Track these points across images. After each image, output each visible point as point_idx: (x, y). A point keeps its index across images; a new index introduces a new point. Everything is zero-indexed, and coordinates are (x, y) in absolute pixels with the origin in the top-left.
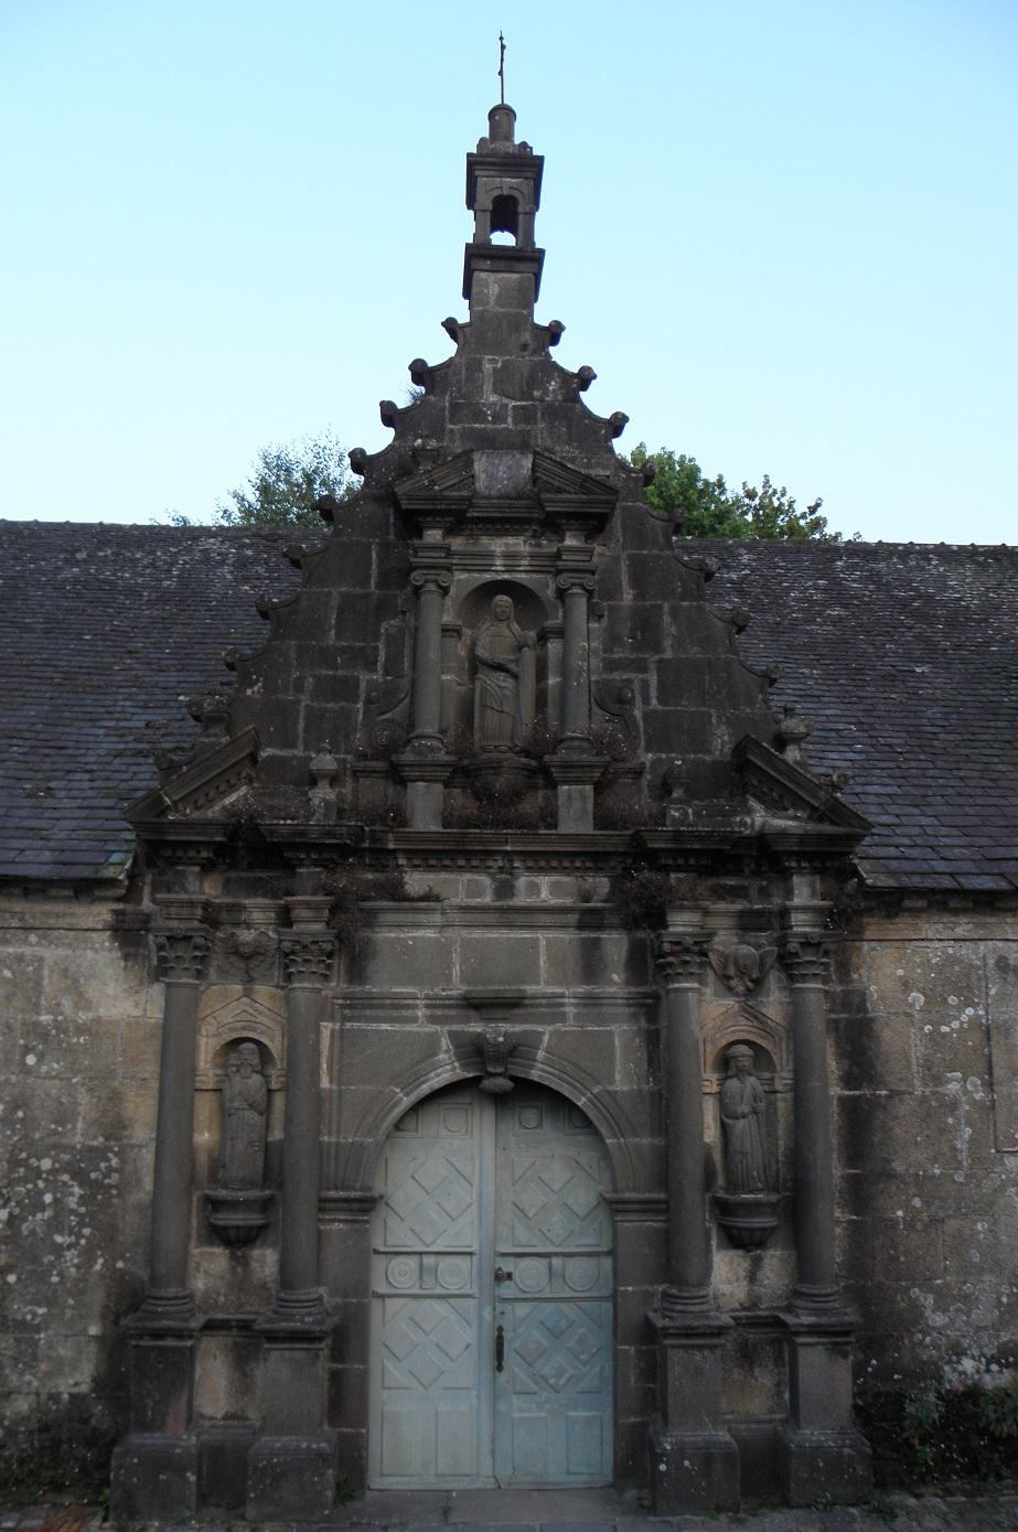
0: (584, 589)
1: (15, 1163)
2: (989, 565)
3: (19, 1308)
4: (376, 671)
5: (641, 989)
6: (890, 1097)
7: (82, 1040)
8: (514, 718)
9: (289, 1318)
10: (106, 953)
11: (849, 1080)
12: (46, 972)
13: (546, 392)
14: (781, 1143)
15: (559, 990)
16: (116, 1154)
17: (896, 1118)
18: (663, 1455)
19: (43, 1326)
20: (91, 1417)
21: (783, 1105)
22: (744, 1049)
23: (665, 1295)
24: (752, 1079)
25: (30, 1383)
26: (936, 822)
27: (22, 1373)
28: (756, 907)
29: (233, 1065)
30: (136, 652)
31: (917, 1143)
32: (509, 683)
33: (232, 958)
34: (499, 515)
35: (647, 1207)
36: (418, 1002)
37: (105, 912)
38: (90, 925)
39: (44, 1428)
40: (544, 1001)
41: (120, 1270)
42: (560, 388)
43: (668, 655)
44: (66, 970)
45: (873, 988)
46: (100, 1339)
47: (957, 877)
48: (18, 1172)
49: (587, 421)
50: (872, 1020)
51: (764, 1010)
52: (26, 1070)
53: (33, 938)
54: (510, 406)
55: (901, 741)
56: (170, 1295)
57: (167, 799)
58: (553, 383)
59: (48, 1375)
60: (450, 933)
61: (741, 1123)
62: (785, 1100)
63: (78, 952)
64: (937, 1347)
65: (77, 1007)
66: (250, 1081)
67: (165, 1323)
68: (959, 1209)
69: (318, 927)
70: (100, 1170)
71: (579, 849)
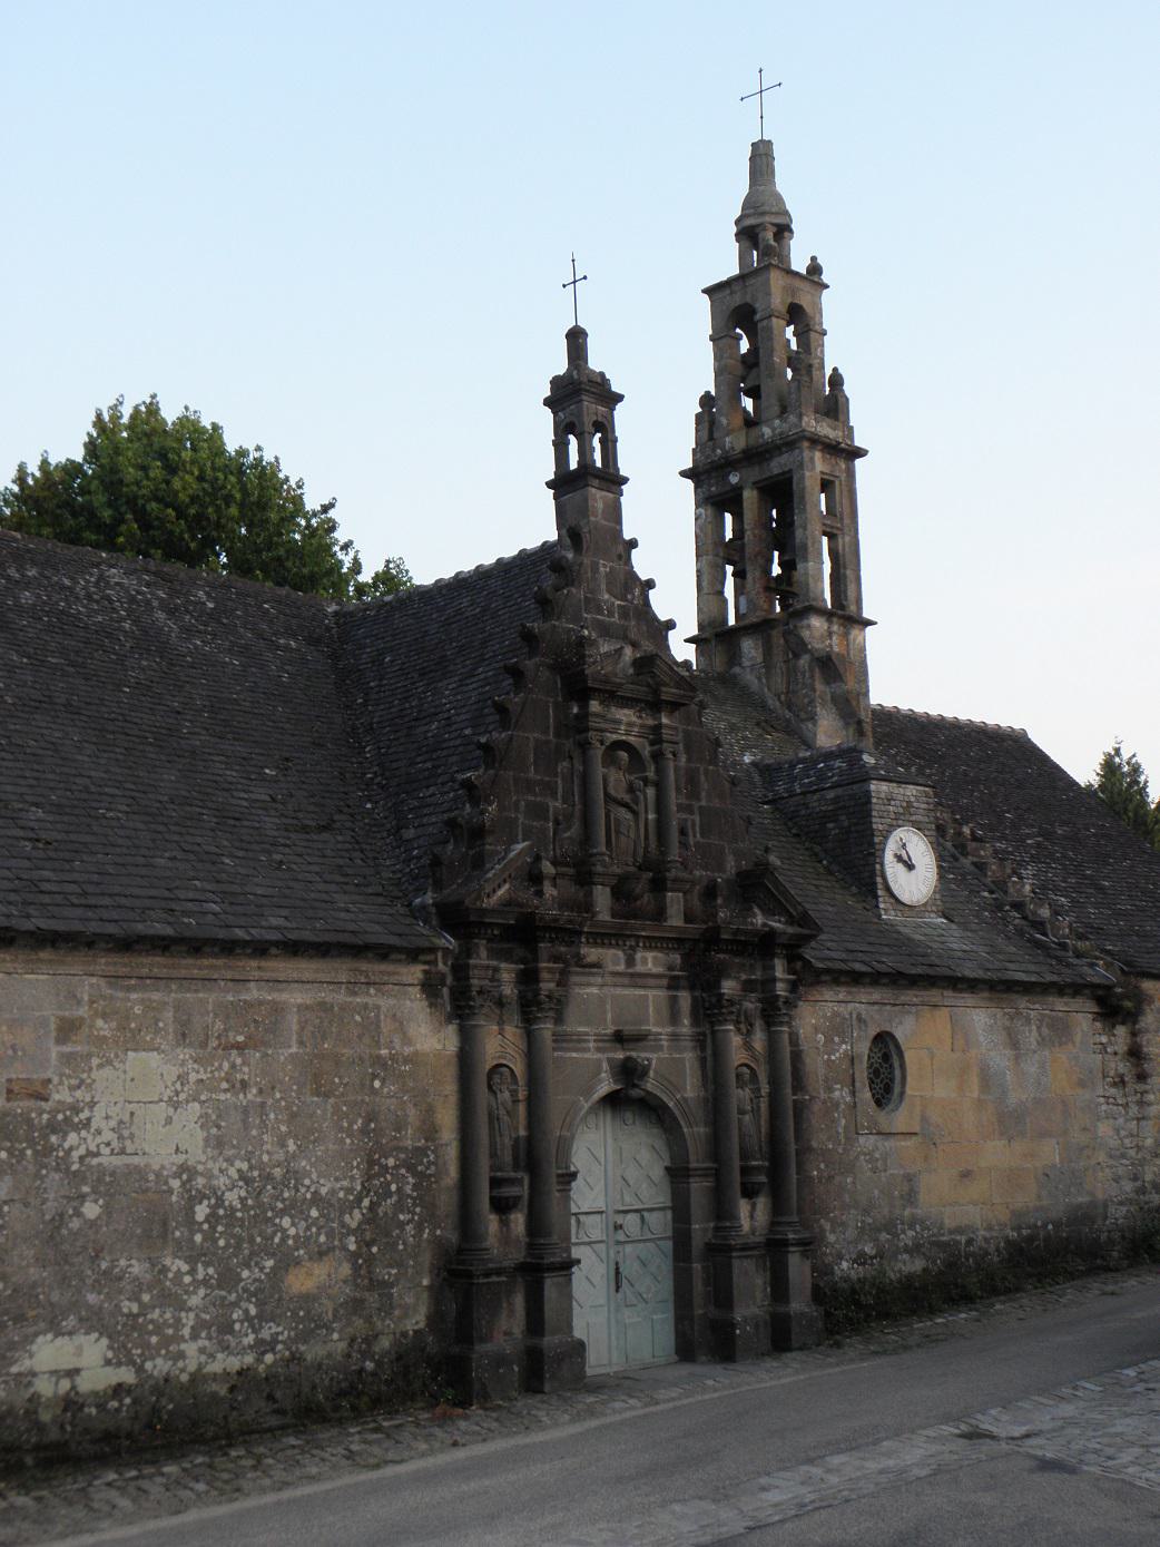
1: (371, 1163)
4: (557, 800)
5: (698, 1030)
6: (810, 1100)
12: (382, 1017)
15: (660, 1030)
22: (745, 1069)
25: (389, 1325)
27: (383, 1320)
31: (822, 1129)
32: (629, 816)
43: (703, 803)
46: (430, 1288)
52: (374, 1091)
53: (372, 991)
59: (400, 1319)
65: (403, 1044)
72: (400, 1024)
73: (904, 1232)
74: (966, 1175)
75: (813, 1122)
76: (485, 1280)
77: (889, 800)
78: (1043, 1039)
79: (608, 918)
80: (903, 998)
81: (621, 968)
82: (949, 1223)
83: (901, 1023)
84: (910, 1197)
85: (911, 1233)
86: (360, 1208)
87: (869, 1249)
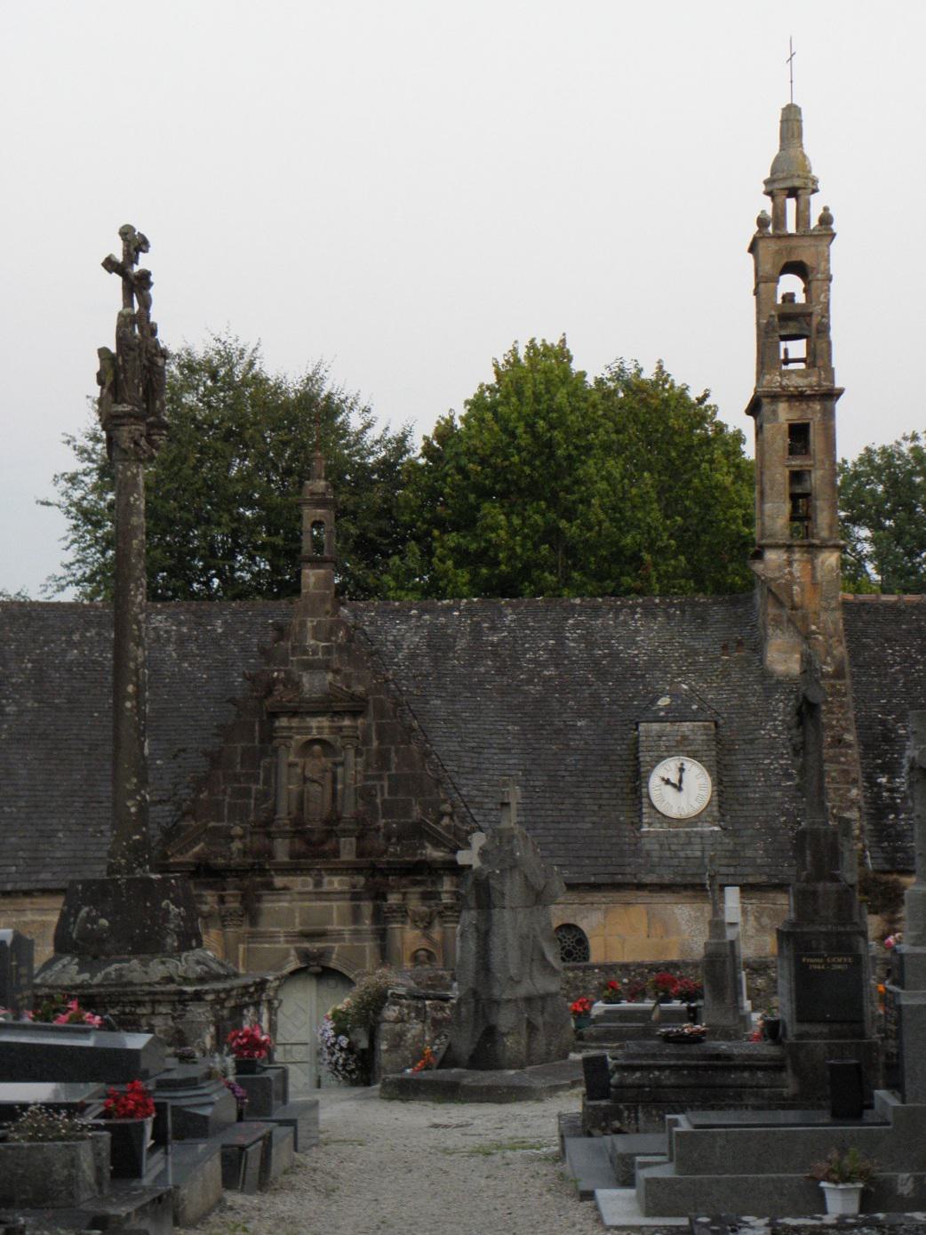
5: (379, 927)
22: (423, 953)
32: (319, 789)
43: (393, 772)
79: (286, 859)
80: (589, 899)
81: (310, 888)
83: (587, 917)
86: (657, 1003)
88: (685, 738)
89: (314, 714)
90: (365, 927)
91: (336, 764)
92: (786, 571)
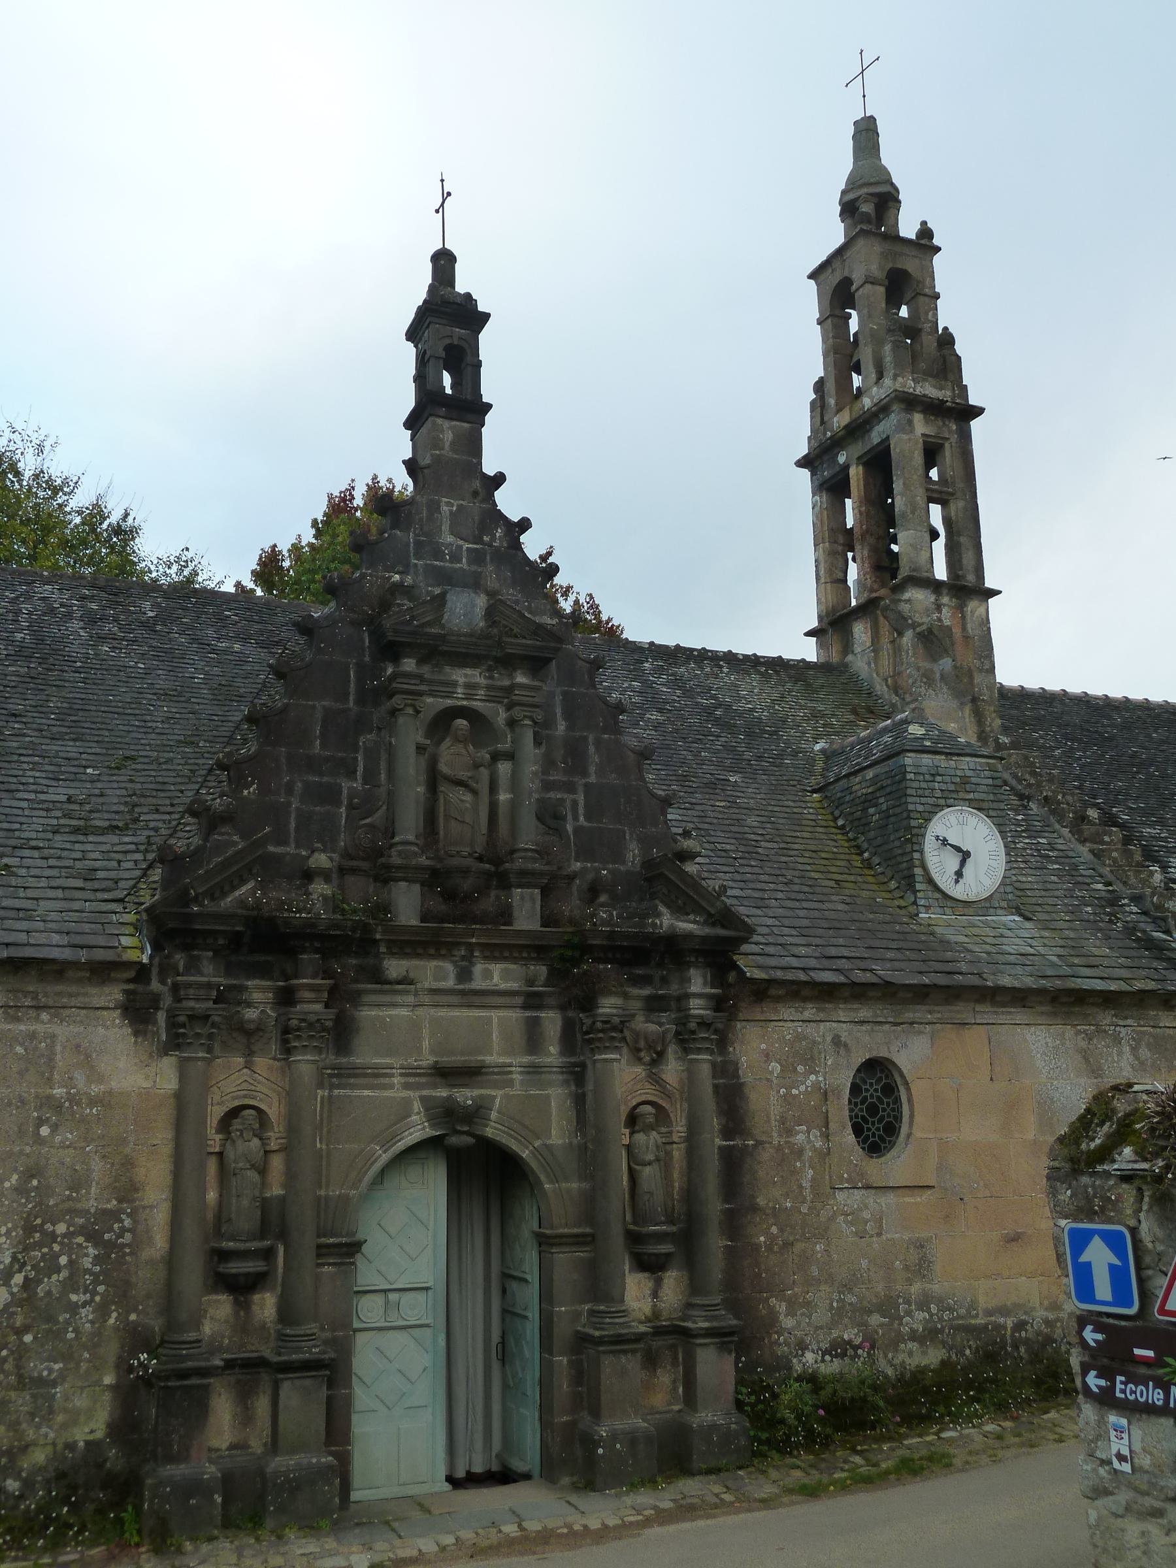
0: (533, 721)
1: (29, 1229)
2: (770, 676)
3: (35, 1366)
4: (356, 779)
5: (573, 1060)
6: (755, 1146)
7: (94, 1111)
8: (473, 827)
9: (299, 1350)
10: (117, 1029)
11: (727, 1133)
12: (58, 1048)
13: (493, 538)
14: (676, 1185)
15: (508, 1061)
16: (129, 1215)
17: (759, 1163)
18: (600, 1441)
19: (59, 1380)
20: (105, 1461)
21: (678, 1153)
22: (648, 1109)
23: (592, 1313)
24: (654, 1133)
25: (46, 1435)
26: (777, 923)
27: (38, 1427)
28: (660, 992)
29: (237, 1130)
30: (20, 716)
31: (775, 1183)
32: (468, 797)
33: (235, 1035)
34: (464, 650)
35: (579, 1240)
36: (394, 1071)
37: (116, 991)
38: (102, 1004)
39: (61, 1475)
40: (496, 1070)
41: (133, 1322)
42: (505, 535)
43: (592, 779)
44: (78, 1046)
45: (744, 1059)
46: (114, 1388)
47: (808, 972)
48: (34, 1238)
49: (527, 568)
50: (743, 1084)
51: (664, 1076)
52: (39, 1140)
53: (45, 1016)
54: (464, 548)
55: (733, 847)
56: (192, 1339)
57: (192, 891)
58: (499, 531)
59: (64, 1426)
60: (420, 1011)
61: (647, 1170)
62: (679, 1149)
63: (90, 1029)
64: (787, 1344)
65: (89, 1081)
66: (251, 1143)
67: (190, 1364)
68: (804, 1234)
69: (318, 1007)
70: (114, 1232)
71: (529, 943)
72: (85, 1057)
73: (909, 1313)
74: (1014, 1239)
75: (761, 1173)
76: (178, 1383)
77: (933, 775)
78: (1142, 1063)
80: (909, 1015)
82: (983, 1302)
84: (921, 1268)
85: (921, 1315)
87: (850, 1334)
88: (965, 780)
89: (464, 659)
90: (549, 1060)
91: (496, 757)
92: (935, 616)
